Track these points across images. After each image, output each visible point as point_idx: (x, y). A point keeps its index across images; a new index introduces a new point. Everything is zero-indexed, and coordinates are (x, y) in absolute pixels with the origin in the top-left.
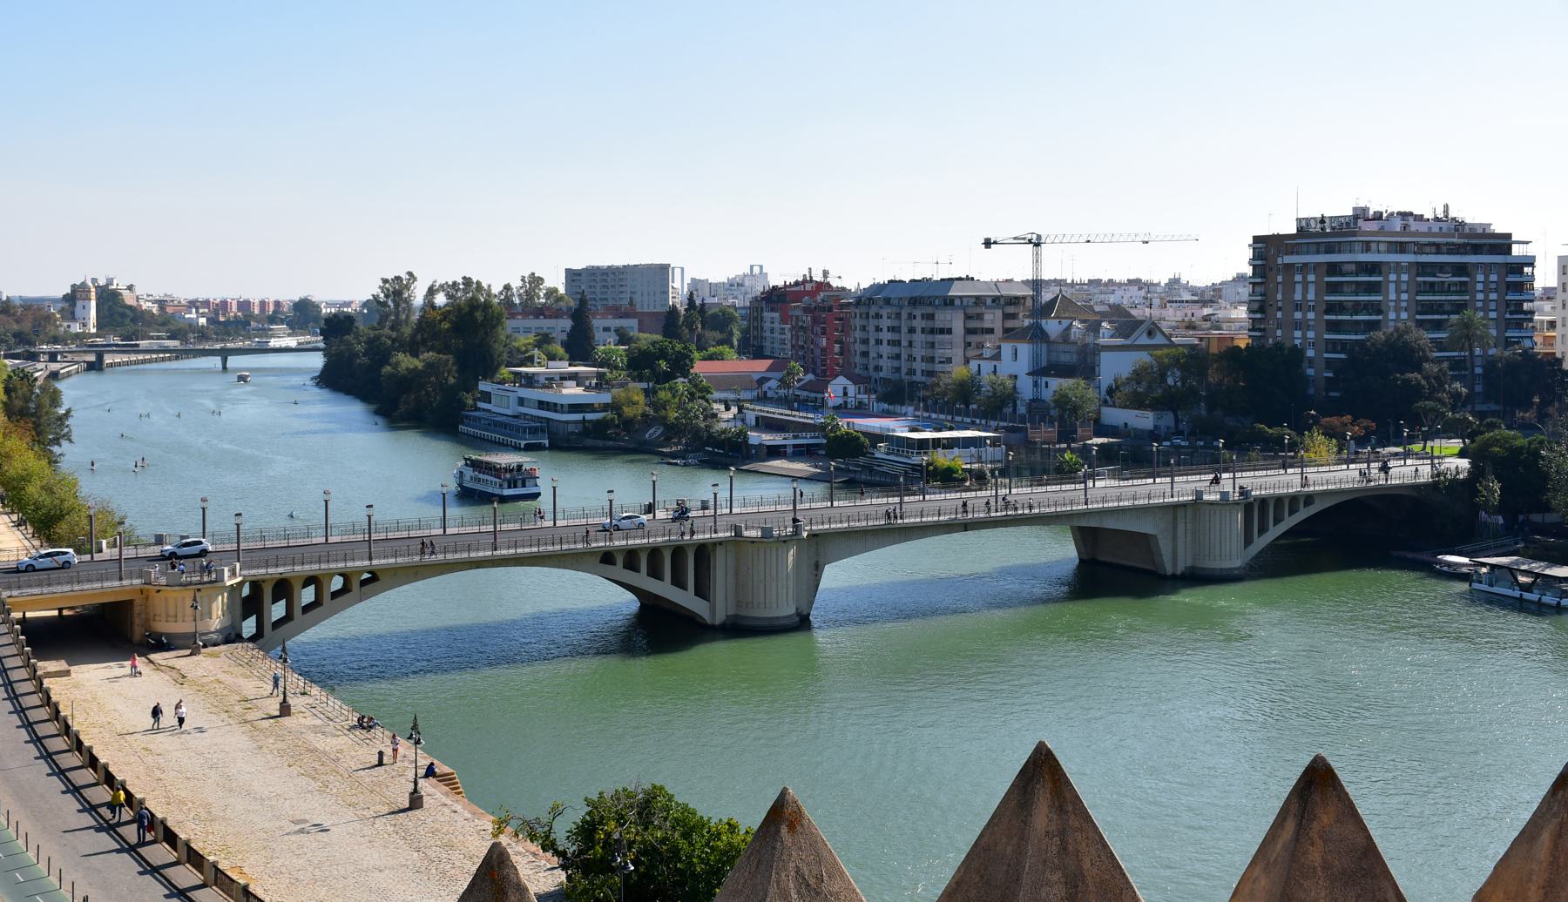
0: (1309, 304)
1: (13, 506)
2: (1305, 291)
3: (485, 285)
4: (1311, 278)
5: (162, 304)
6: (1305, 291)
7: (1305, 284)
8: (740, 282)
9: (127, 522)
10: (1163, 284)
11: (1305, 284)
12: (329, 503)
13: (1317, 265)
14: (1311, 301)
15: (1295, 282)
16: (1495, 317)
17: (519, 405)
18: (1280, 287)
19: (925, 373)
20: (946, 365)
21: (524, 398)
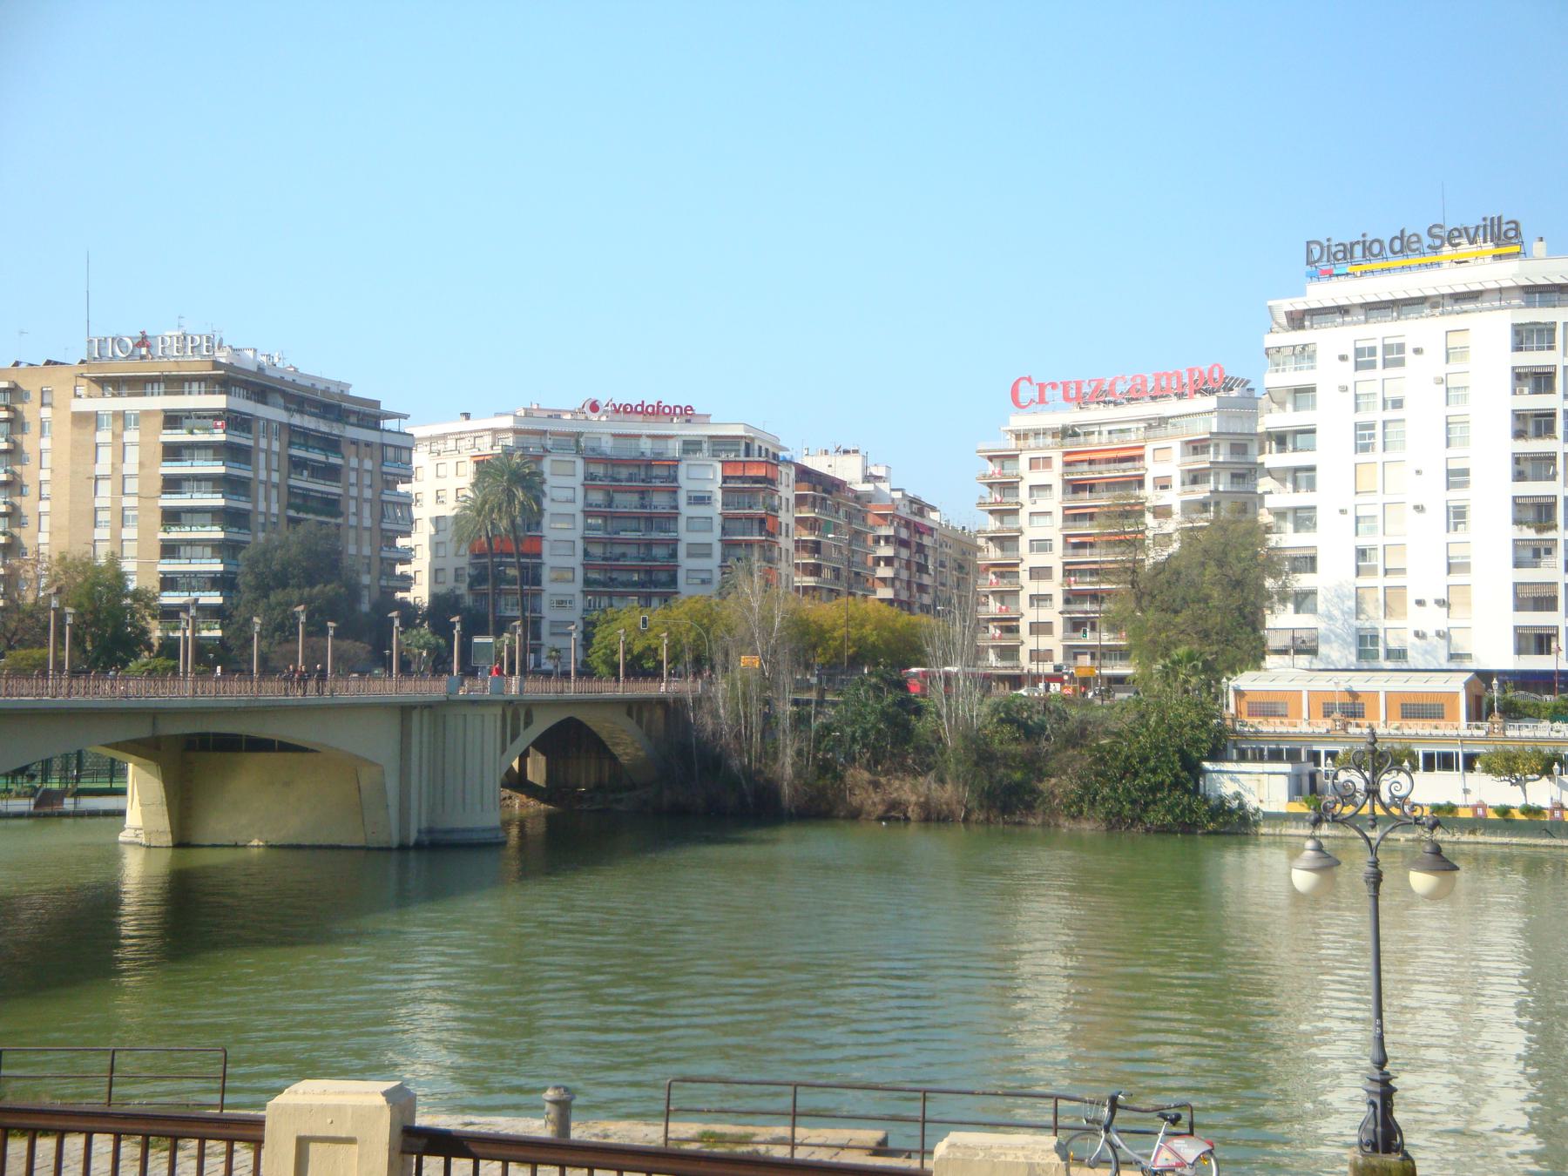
4: (131, 436)
13: (147, 413)
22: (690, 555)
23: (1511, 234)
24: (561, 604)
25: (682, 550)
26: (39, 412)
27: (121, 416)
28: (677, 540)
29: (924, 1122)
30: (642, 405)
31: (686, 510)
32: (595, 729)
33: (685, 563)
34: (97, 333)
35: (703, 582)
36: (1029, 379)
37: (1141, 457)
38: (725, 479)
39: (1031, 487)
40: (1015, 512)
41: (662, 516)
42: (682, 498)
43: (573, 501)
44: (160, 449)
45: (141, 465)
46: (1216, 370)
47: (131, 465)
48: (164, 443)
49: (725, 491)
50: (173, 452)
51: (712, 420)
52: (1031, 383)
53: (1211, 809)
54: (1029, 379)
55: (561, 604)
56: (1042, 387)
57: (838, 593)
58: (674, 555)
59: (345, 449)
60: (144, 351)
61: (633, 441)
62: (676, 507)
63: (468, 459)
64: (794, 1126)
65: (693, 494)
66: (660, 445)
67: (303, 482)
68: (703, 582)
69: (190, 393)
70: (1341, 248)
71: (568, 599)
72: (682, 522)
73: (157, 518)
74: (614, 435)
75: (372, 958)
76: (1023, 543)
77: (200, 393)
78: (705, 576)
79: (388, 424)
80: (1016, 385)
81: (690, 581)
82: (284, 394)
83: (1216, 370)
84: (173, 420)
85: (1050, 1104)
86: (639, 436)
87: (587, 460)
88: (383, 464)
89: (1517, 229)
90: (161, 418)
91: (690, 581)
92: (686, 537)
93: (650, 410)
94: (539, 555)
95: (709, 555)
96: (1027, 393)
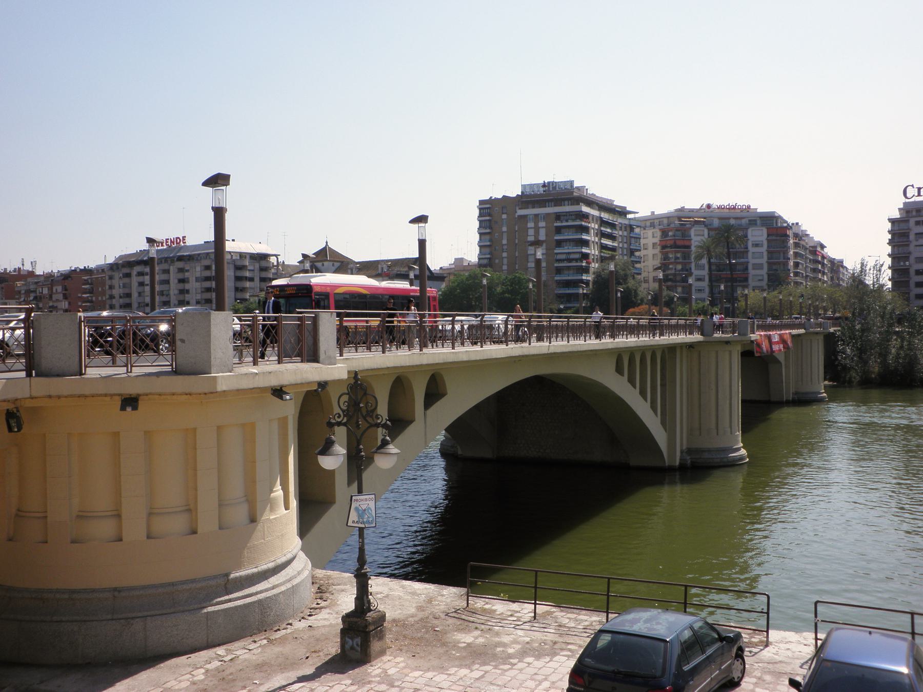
12: (230, 196)
13: (548, 215)
22: (754, 269)
24: (700, 290)
25: (750, 267)
26: (502, 216)
27: (536, 216)
28: (748, 262)
29: (536, 588)
30: (729, 205)
31: (751, 249)
32: (387, 405)
33: (752, 272)
35: (760, 280)
36: (912, 186)
38: (768, 235)
39: (916, 234)
40: (908, 245)
41: (741, 252)
42: (750, 244)
43: (762, 235)
44: (554, 229)
45: (546, 235)
49: (769, 241)
52: (913, 188)
53: (686, 452)
55: (700, 290)
56: (919, 189)
58: (747, 269)
61: (727, 221)
62: (747, 248)
63: (658, 230)
64: (535, 604)
65: (754, 243)
66: (739, 222)
67: (605, 241)
68: (760, 280)
69: (564, 205)
71: (702, 289)
72: (750, 255)
76: (912, 258)
77: (568, 205)
78: (760, 278)
79: (629, 216)
82: (597, 204)
84: (558, 217)
87: (709, 230)
88: (630, 233)
92: (752, 261)
93: (732, 207)
96: (911, 192)
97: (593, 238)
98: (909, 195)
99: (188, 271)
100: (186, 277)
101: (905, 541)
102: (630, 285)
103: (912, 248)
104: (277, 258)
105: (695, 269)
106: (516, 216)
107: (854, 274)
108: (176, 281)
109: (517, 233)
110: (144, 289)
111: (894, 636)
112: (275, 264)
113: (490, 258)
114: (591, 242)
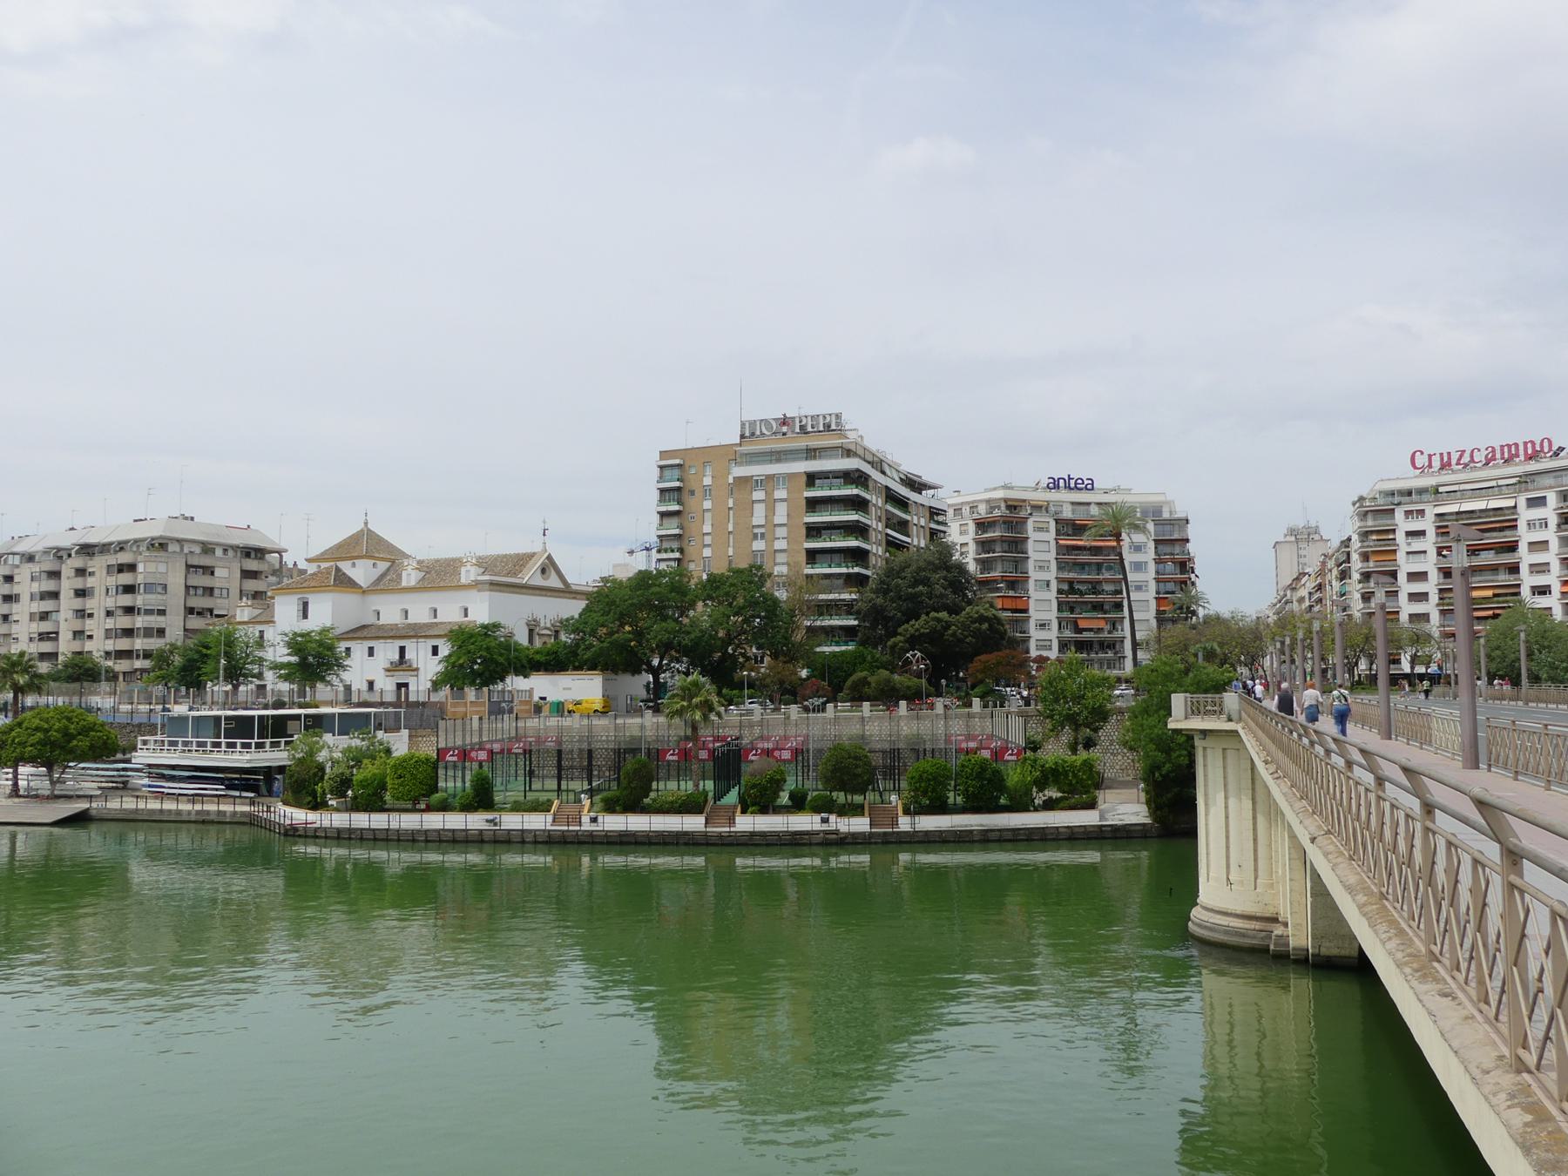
0: (756, 531)
1: (736, 637)
2: (771, 511)
3: (1181, 1127)
4: (781, 493)
5: (460, 627)
6: (771, 511)
7: (771, 504)
8: (129, 786)
9: (1422, 696)
10: (309, 572)
11: (771, 504)
12: (628, 1018)
13: (791, 476)
14: (759, 526)
15: (753, 502)
16: (410, 700)
17: (1426, 580)
18: (708, 516)
19: (120, 589)
20: (1507, 533)
21: (1518, 572)
23: (1089, 487)
34: (748, 417)
37: (1515, 527)
44: (804, 502)
46: (1546, 444)
47: (781, 515)
48: (807, 499)
50: (813, 504)
51: (1132, 492)
54: (1422, 453)
57: (1210, 656)
59: (913, 509)
60: (785, 429)
70: (1051, 481)
73: (803, 557)
74: (1073, 503)
75: (1209, 1143)
80: (1415, 453)
81: (1049, 643)
83: (1546, 444)
84: (811, 479)
85: (546, 787)
86: (1089, 504)
89: (1092, 484)
90: (804, 478)
91: (1049, 643)
94: (1026, 611)
95: (1410, 595)
96: (1421, 461)
97: (874, 522)
98: (1418, 464)
99: (92, 574)
100: (89, 585)
101: (905, 1074)
102: (103, 684)
103: (1401, 556)
104: (281, 557)
105: (1036, 590)
106: (731, 480)
107: (340, 666)
108: (70, 635)
109: (731, 512)
110: (10, 630)
111: (201, 771)
112: (277, 566)
113: (679, 560)
114: (910, 524)
